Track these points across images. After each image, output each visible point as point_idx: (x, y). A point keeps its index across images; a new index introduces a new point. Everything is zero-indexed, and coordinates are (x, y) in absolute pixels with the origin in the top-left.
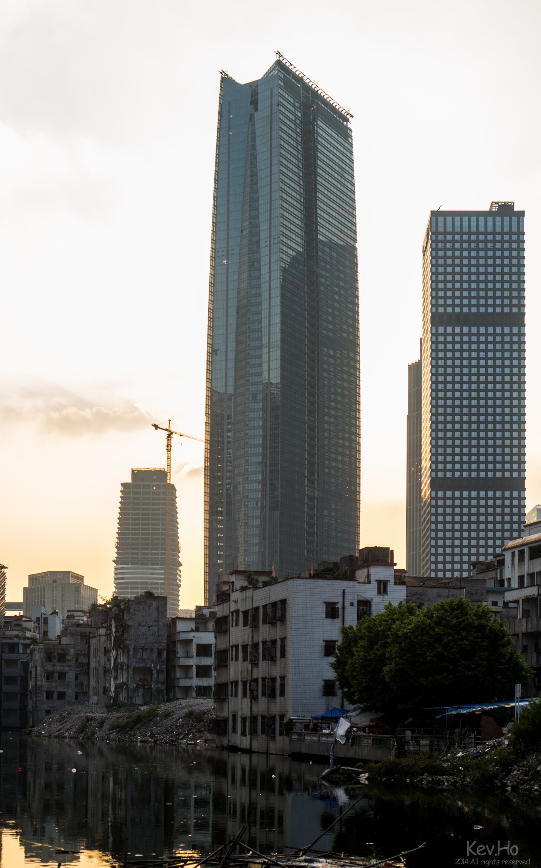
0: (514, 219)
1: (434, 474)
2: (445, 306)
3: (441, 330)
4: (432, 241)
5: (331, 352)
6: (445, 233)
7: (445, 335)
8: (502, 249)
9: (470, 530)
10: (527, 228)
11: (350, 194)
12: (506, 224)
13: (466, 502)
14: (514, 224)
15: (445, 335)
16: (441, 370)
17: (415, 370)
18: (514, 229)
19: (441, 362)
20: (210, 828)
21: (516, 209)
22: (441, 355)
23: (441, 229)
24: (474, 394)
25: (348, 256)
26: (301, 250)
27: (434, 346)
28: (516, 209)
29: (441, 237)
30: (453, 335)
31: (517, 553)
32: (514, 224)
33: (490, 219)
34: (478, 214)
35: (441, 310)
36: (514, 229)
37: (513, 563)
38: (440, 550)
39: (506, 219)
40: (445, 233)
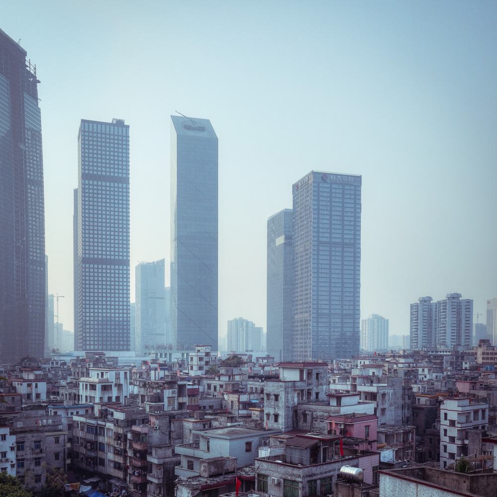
0: (124, 129)
1: (83, 171)
2: (89, 170)
3: (87, 182)
4: (82, 135)
5: (33, 188)
6: (89, 132)
7: (89, 185)
8: (114, 156)
9: (94, 300)
10: (131, 134)
11: (38, 122)
12: (120, 131)
13: (96, 270)
14: (124, 131)
15: (89, 185)
16: (87, 231)
17: (76, 191)
18: (124, 134)
19: (87, 227)
20: (216, 417)
21: (125, 124)
22: (87, 207)
23: (87, 130)
24: (104, 192)
25: (37, 136)
26: (8, 129)
27: (83, 146)
28: (125, 124)
29: (87, 134)
30: (93, 185)
31: (84, 385)
32: (124, 131)
33: (112, 127)
34: (106, 124)
35: (87, 172)
36: (124, 134)
37: (83, 388)
38: (88, 310)
39: (120, 128)
40: (89, 132)
